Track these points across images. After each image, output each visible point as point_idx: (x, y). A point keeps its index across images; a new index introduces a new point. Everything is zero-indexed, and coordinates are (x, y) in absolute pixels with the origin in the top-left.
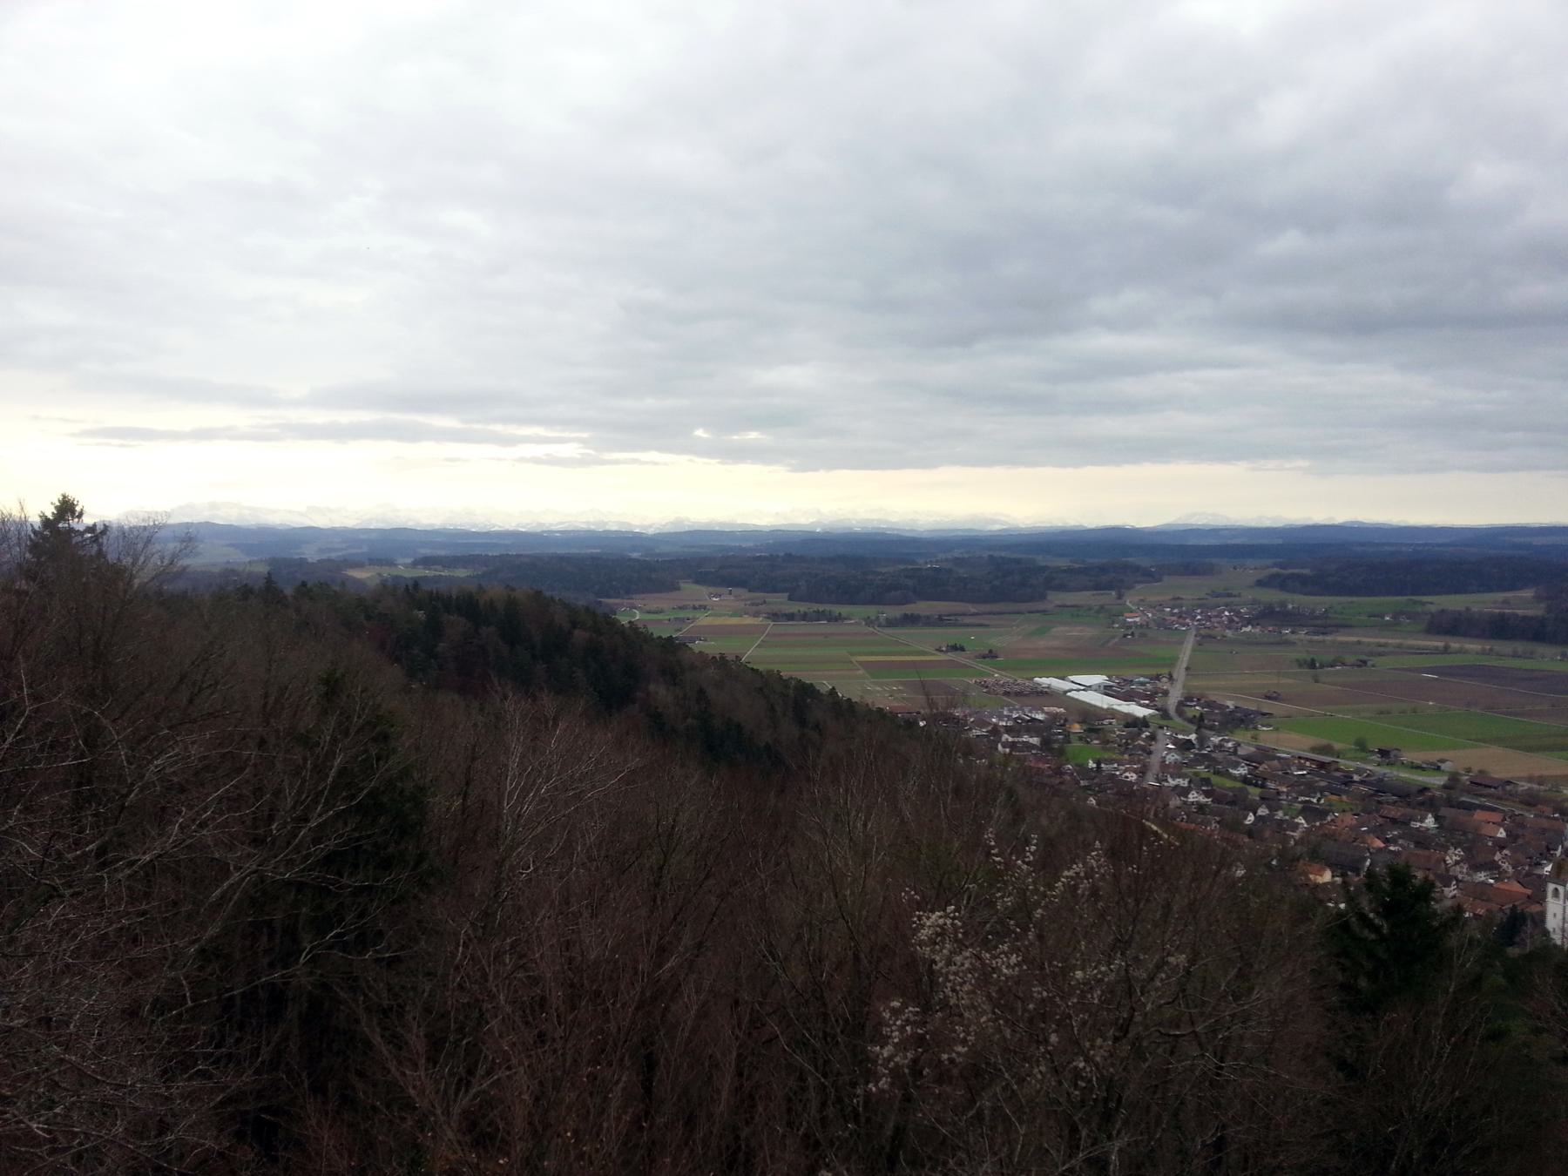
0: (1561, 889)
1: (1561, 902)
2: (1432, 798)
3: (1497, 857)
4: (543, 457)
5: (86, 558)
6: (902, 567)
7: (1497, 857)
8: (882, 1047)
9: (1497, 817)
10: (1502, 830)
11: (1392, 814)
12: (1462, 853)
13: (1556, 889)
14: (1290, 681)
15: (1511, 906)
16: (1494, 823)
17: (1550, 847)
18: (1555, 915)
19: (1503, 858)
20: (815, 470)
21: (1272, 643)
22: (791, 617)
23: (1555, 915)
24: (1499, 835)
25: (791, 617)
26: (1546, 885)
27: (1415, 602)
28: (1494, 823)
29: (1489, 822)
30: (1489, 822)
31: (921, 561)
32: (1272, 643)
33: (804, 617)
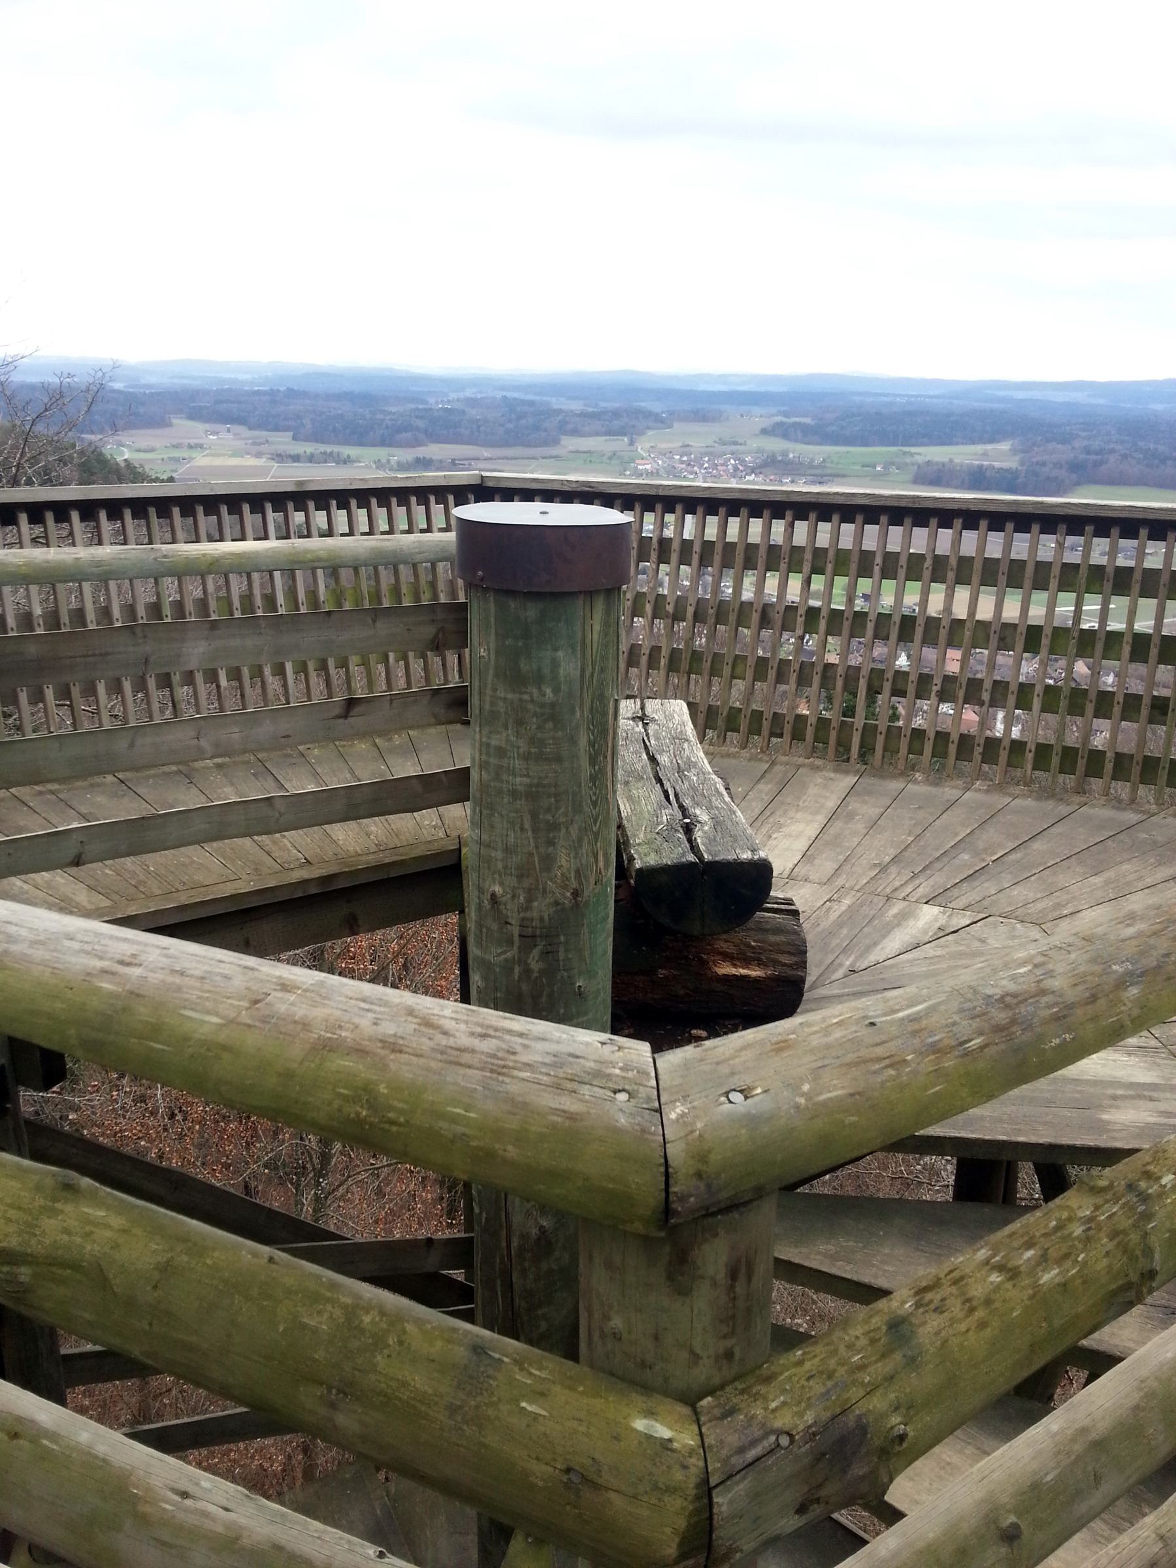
6: (413, 406)
22: (296, 458)
25: (296, 458)
27: (905, 453)
31: (432, 400)
33: (311, 459)
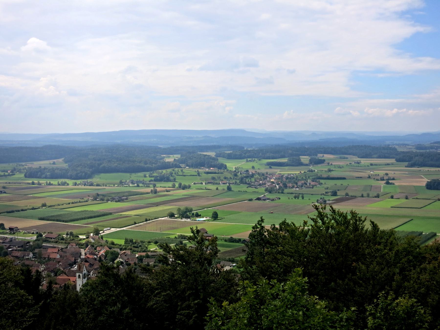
0: (81, 275)
1: (81, 280)
2: (31, 246)
3: (57, 266)
4: (414, 151)
5: (13, 239)
7: (57, 266)
8: (425, 325)
9: (56, 250)
10: (58, 255)
11: (16, 255)
12: (44, 267)
13: (79, 275)
14: (353, 189)
15: (64, 284)
16: (55, 253)
17: (76, 259)
18: (80, 285)
19: (59, 266)
20: (119, 131)
21: (380, 165)
23: (80, 285)
24: (57, 257)
26: (76, 274)
28: (55, 253)
29: (53, 253)
30: (53, 253)
32: (380, 165)
